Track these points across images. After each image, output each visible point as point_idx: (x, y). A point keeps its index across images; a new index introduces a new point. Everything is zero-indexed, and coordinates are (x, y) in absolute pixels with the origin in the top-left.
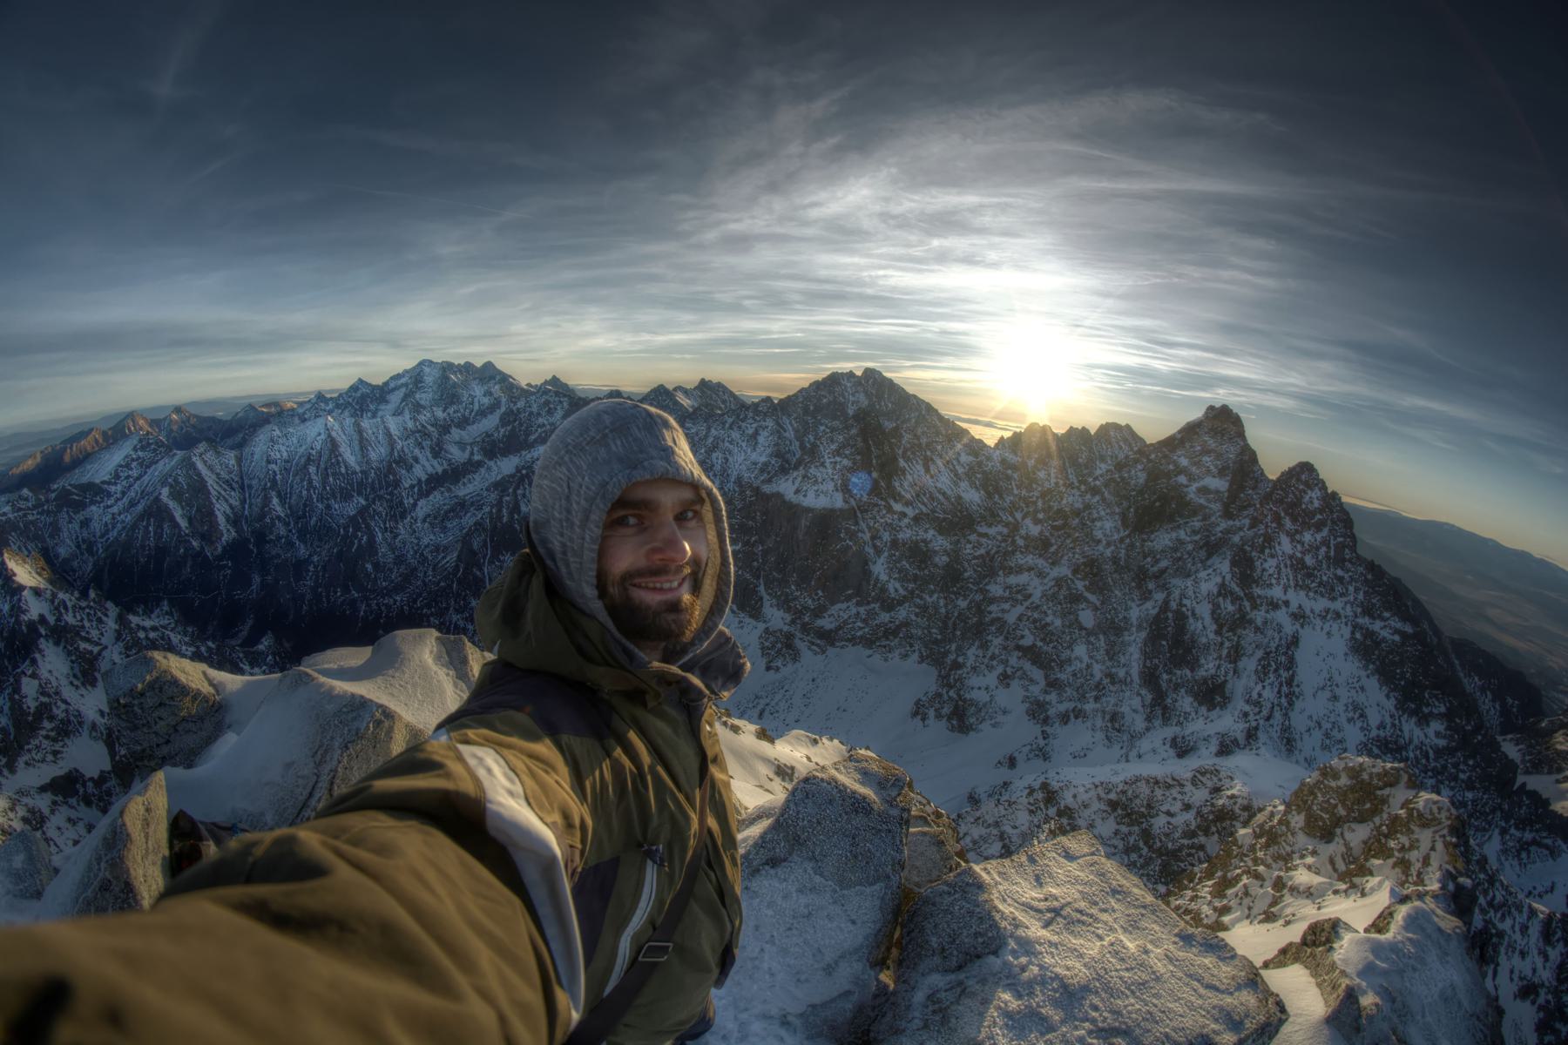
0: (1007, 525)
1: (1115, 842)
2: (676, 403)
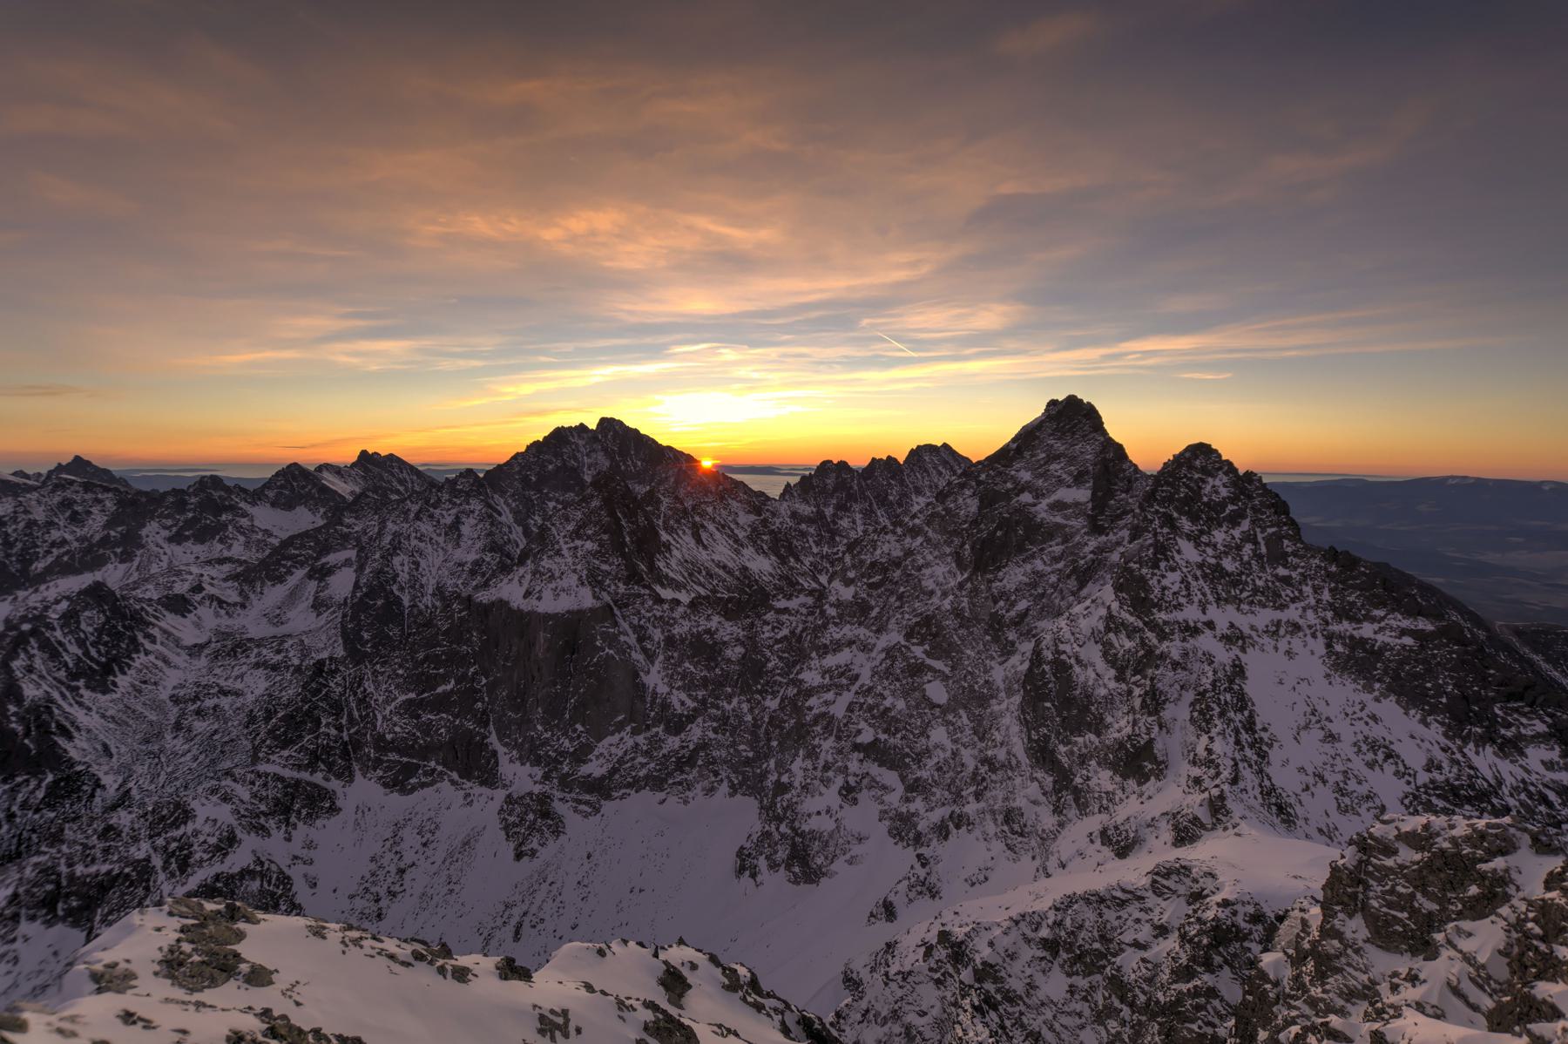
0: (811, 593)
2: (325, 490)
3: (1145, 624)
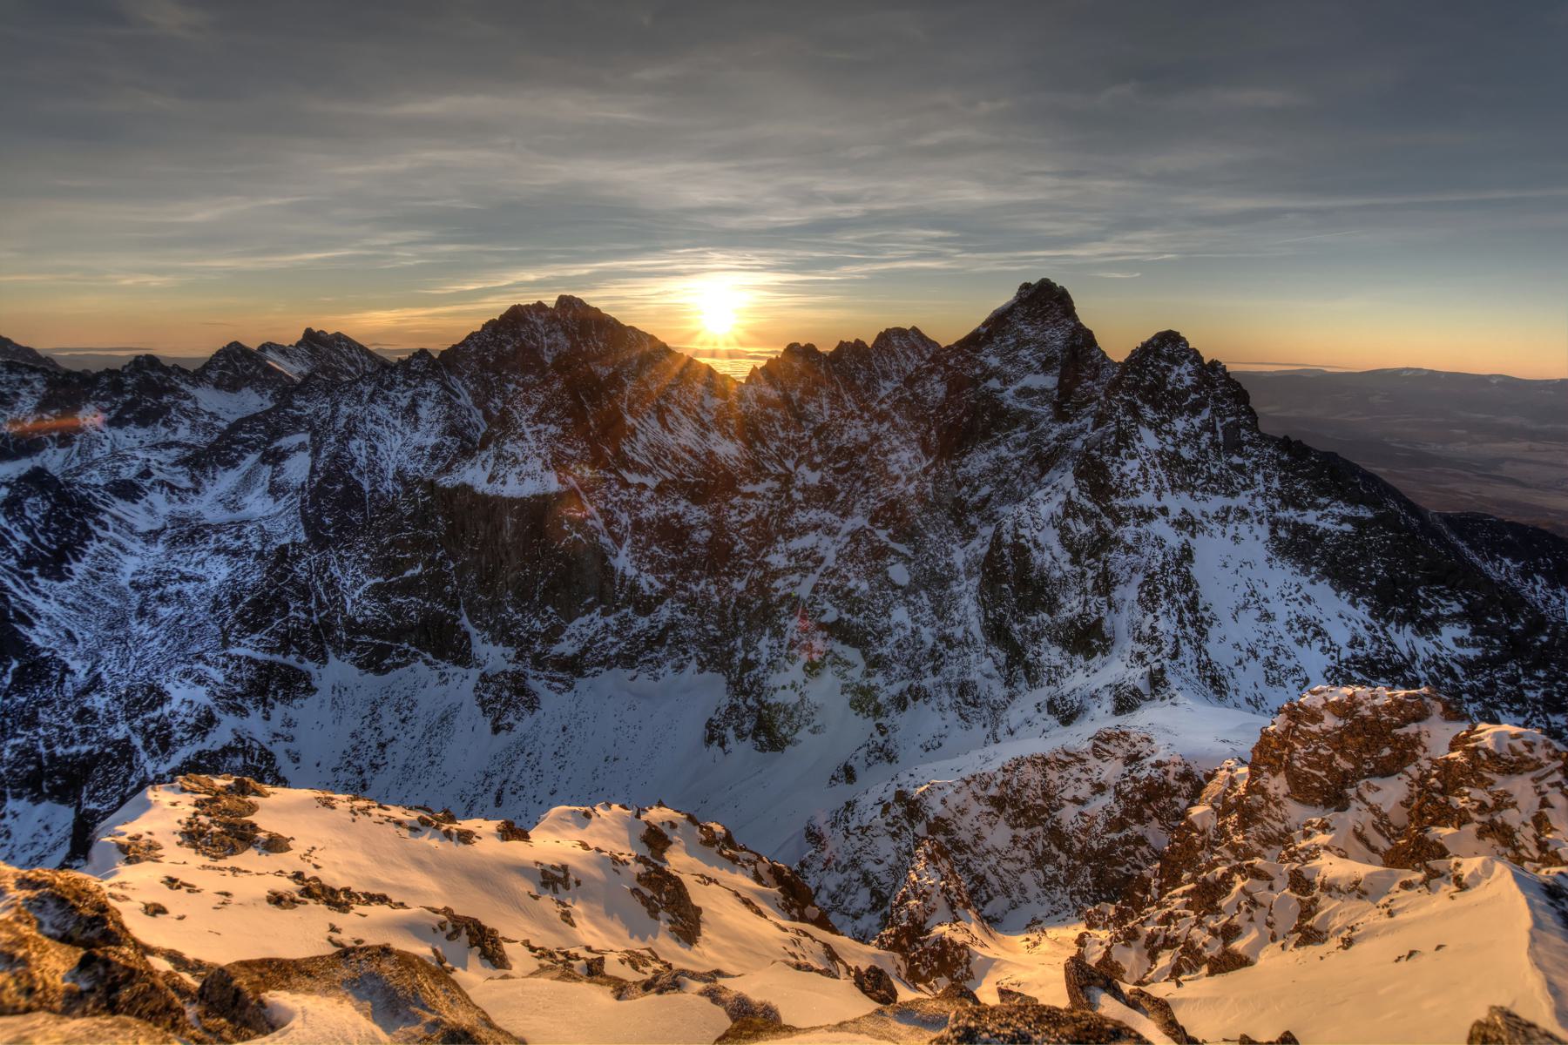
0: (778, 477)
1: (1016, 853)
2: (270, 370)
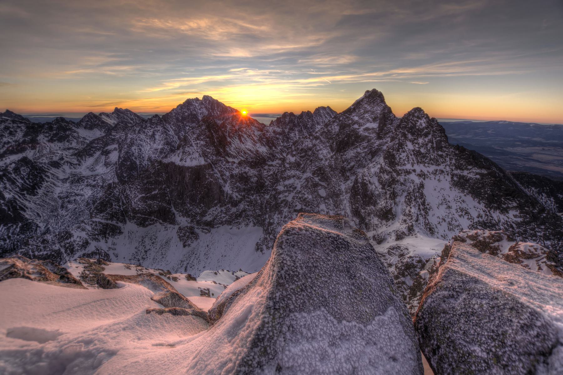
0: (280, 159)
2: (103, 122)
3: (393, 170)
